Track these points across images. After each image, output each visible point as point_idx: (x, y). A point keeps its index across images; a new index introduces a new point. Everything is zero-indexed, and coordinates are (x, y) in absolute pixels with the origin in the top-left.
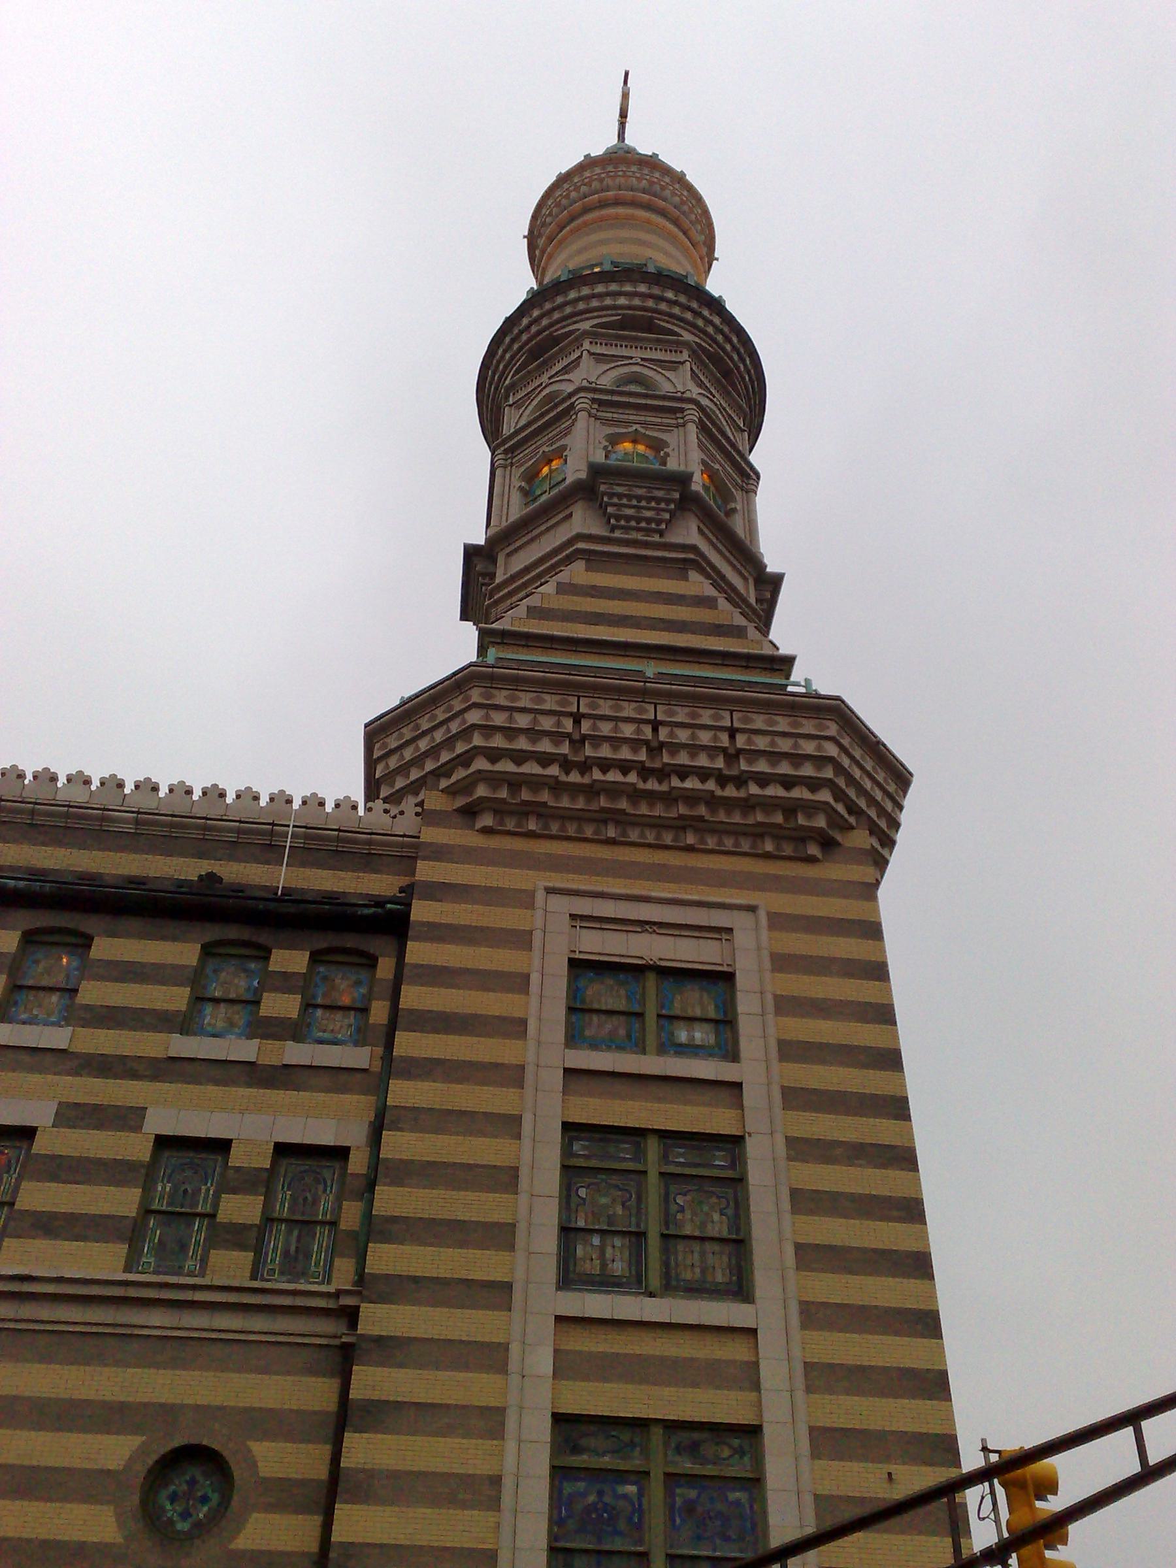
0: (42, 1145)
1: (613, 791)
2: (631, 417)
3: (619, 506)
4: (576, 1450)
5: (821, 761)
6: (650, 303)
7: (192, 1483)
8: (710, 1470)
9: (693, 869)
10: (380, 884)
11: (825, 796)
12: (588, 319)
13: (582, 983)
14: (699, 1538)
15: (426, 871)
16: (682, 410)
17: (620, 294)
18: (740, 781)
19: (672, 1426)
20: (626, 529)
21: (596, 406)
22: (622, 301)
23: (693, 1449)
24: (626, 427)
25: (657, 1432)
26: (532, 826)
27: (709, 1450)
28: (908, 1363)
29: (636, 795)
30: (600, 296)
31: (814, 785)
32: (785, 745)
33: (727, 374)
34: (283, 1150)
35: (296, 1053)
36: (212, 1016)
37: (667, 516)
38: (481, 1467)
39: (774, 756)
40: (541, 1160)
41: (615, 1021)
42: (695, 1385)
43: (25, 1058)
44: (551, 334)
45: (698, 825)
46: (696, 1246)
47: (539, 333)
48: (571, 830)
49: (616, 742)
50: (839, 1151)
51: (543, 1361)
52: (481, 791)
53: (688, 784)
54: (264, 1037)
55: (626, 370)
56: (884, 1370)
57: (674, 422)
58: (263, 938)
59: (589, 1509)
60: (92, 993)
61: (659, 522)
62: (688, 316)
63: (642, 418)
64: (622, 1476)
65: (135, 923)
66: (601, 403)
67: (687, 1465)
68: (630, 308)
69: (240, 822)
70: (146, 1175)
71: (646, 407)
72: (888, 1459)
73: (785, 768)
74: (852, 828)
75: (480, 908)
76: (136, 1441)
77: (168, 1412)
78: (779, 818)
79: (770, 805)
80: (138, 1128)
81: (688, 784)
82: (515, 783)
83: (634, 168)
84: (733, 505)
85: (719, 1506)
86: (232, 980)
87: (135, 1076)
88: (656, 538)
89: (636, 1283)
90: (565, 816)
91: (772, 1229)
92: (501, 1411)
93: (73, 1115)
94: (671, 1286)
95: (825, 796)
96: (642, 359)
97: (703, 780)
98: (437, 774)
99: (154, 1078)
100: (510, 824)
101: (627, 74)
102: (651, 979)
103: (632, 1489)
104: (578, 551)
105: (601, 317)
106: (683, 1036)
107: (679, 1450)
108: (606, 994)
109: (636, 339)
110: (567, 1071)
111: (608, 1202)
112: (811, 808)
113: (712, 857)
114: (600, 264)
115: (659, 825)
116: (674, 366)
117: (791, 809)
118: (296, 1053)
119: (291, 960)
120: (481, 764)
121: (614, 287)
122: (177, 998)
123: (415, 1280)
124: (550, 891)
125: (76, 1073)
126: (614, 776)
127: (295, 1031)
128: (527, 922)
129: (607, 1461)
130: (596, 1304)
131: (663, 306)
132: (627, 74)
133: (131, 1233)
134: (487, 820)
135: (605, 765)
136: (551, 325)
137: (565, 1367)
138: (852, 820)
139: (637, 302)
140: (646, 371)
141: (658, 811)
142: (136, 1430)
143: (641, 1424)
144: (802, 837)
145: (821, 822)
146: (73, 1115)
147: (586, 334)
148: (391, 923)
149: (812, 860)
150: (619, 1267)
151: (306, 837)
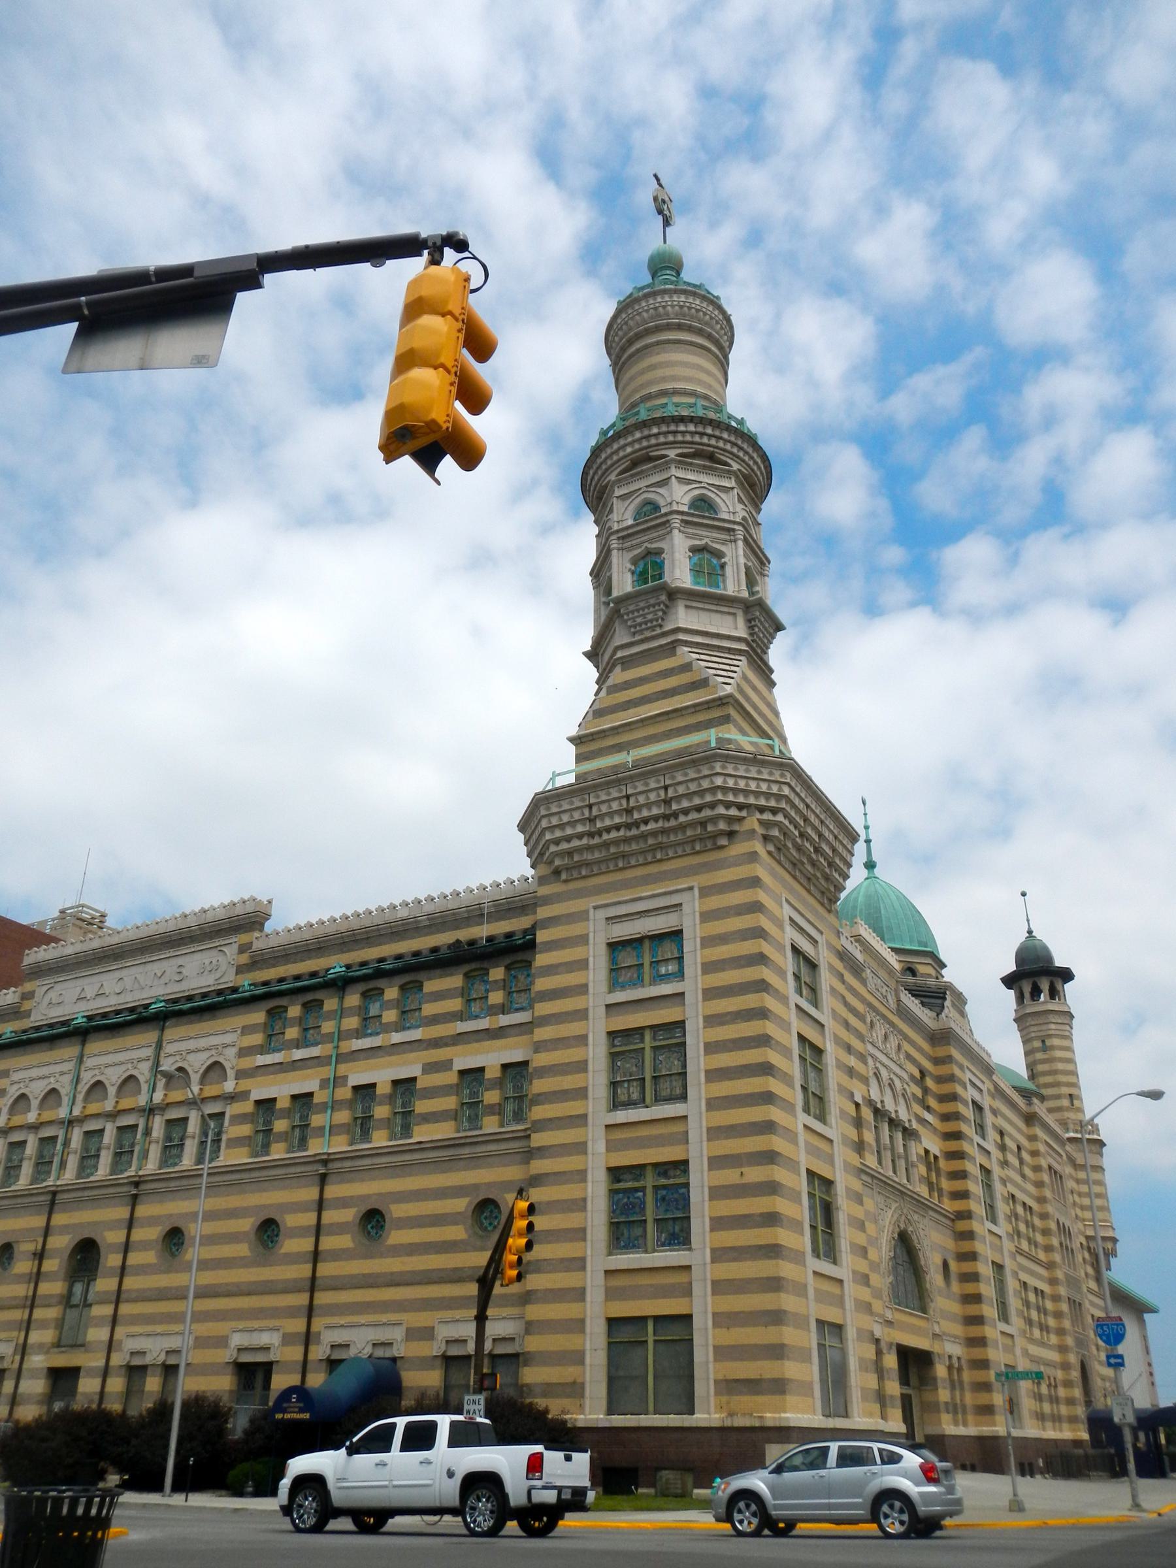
0: (420, 1084)
1: (616, 842)
3: (634, 619)
4: (619, 1181)
7: (491, 1212)
8: (671, 1181)
9: (665, 872)
10: (523, 922)
13: (616, 954)
14: (667, 1210)
15: (543, 913)
16: (734, 530)
17: (626, 445)
18: (675, 815)
19: (655, 1165)
20: (641, 632)
22: (629, 450)
23: (665, 1174)
25: (649, 1168)
26: (584, 873)
27: (671, 1173)
28: (754, 1119)
29: (627, 840)
32: (693, 787)
33: (711, 457)
34: (505, 1067)
35: (505, 1020)
36: (475, 1008)
37: (660, 613)
38: (577, 1194)
39: (689, 796)
40: (597, 1052)
41: (632, 970)
42: (663, 1146)
43: (407, 1046)
45: (661, 847)
46: (668, 1079)
48: (604, 869)
49: (611, 814)
50: (728, 1018)
51: (601, 1147)
53: (649, 827)
54: (491, 1015)
56: (741, 1125)
58: (485, 965)
59: (626, 1204)
60: (429, 1009)
62: (671, 438)
64: (636, 1190)
65: (438, 972)
66: (623, 538)
67: (663, 1181)
70: (455, 1089)
71: (648, 529)
72: (741, 1166)
73: (697, 801)
75: (566, 927)
76: (355, 1210)
77: (476, 1187)
79: (692, 824)
80: (451, 1069)
81: (649, 827)
82: (570, 853)
85: (676, 1196)
86: (478, 990)
87: (447, 1045)
88: (658, 631)
89: (642, 1102)
90: (599, 862)
91: (697, 1062)
92: (586, 1171)
93: (430, 1068)
94: (658, 1099)
98: (762, 810)
99: (454, 1044)
100: (575, 875)
101: (656, 176)
102: (647, 943)
103: (640, 1194)
106: (663, 970)
107: (659, 1175)
108: (627, 958)
109: (642, 472)
110: (607, 1006)
111: (629, 1065)
112: (714, 820)
113: (673, 861)
114: (613, 425)
115: (643, 852)
117: (703, 824)
118: (505, 1020)
119: (497, 973)
120: (553, 848)
122: (455, 1004)
123: (550, 1120)
124: (595, 908)
125: (426, 1049)
126: (614, 834)
127: (503, 1009)
128: (589, 926)
129: (629, 1185)
130: (622, 1116)
132: (656, 176)
133: (454, 1115)
134: (564, 876)
137: (611, 1147)
138: (744, 813)
139: (637, 446)
140: (710, 494)
142: (467, 1196)
143: (642, 1167)
144: (715, 836)
146: (430, 1068)
148: (530, 946)
150: (635, 1096)
151: (494, 906)
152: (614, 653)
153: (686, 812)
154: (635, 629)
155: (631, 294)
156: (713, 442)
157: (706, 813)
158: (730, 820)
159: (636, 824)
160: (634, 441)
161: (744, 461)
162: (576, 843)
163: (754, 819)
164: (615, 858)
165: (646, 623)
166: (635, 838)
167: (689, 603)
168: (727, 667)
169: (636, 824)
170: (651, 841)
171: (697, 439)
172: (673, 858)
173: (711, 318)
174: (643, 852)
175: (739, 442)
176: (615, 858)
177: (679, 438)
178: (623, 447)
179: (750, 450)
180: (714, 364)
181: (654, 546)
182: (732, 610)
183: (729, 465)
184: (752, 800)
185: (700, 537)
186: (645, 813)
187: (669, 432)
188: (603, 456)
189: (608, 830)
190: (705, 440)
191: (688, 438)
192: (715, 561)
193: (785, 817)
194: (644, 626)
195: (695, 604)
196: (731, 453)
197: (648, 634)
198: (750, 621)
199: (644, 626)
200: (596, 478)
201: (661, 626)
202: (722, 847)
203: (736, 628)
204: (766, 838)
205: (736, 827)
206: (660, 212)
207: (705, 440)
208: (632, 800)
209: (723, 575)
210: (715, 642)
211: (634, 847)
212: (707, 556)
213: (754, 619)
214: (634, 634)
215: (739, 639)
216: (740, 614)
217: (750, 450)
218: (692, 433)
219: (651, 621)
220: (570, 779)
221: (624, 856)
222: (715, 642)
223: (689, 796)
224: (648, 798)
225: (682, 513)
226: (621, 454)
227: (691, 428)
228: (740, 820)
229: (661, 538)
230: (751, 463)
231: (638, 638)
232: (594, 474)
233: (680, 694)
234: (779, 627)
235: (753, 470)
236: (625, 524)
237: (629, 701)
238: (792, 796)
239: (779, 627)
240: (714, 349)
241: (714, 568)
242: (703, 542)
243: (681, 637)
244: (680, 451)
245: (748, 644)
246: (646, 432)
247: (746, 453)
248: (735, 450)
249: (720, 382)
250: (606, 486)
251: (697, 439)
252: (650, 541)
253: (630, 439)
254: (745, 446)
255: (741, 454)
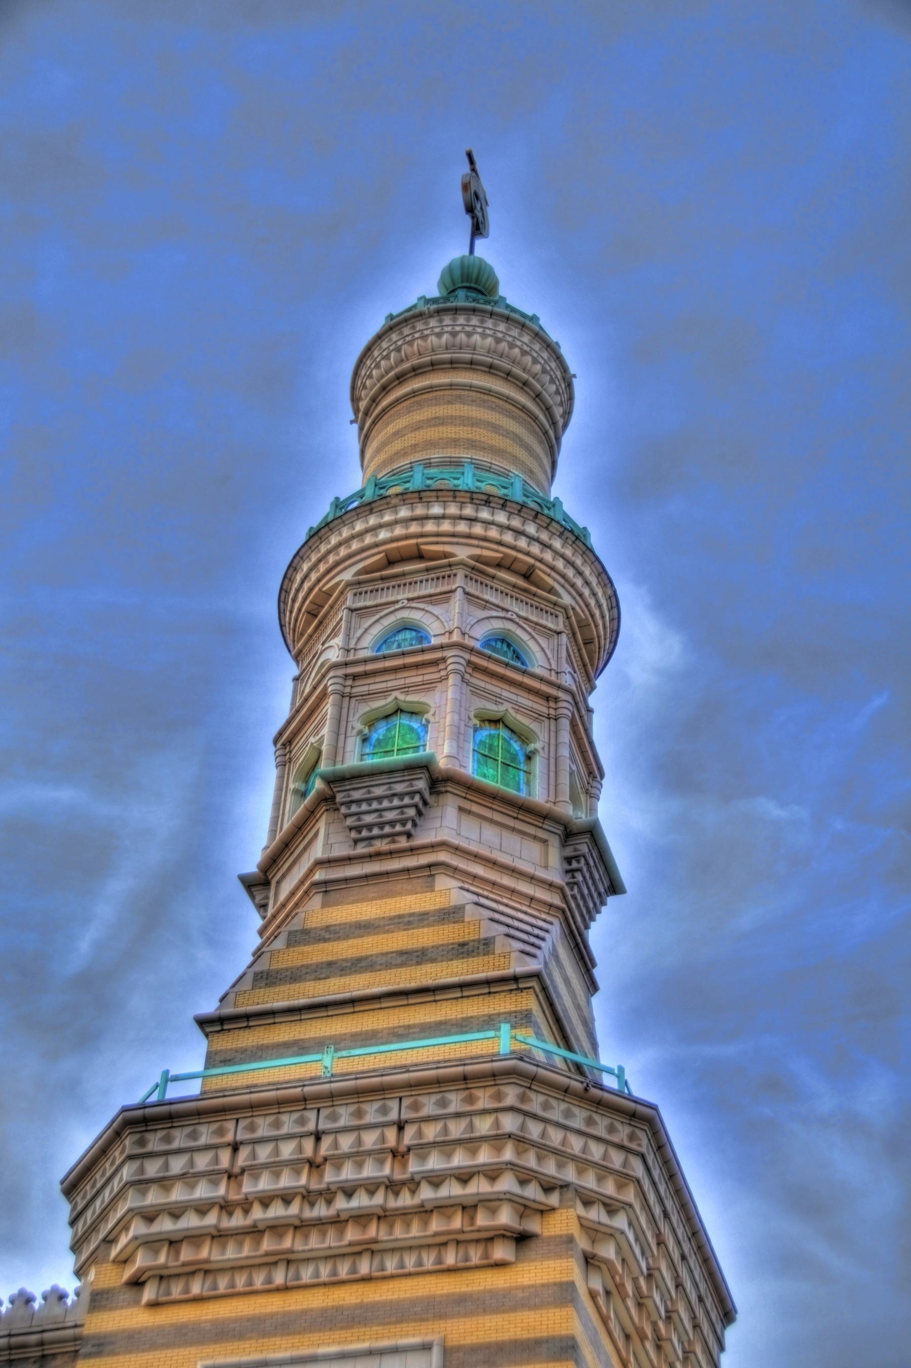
2: (390, 684)
5: (498, 1139)
6: (414, 528)
11: (507, 1184)
12: (345, 569)
16: (556, 699)
18: (413, 1184)
21: (349, 682)
22: (383, 535)
24: (385, 697)
29: (301, 1227)
30: (361, 535)
31: (492, 1173)
32: (457, 1129)
37: (411, 812)
44: (320, 590)
45: (370, 1249)
47: (311, 590)
52: (141, 1260)
53: (354, 1203)
55: (391, 619)
57: (437, 676)
61: (403, 822)
62: (462, 527)
63: (401, 682)
66: (476, 668)
68: (392, 540)
69: (435, 1001)
71: (405, 667)
74: (553, 1209)
78: (457, 1222)
79: (443, 1208)
81: (354, 1203)
83: (433, 323)
84: (532, 746)
88: (403, 843)
95: (507, 1184)
96: (409, 600)
97: (371, 1193)
101: (470, 155)
104: (316, 884)
105: (362, 560)
112: (490, 1203)
115: (333, 1257)
116: (444, 597)
117: (469, 1208)
121: (373, 521)
126: (277, 1211)
131: (430, 527)
132: (470, 155)
134: (149, 1293)
135: (265, 1201)
136: (319, 581)
138: (554, 1199)
139: (399, 531)
140: (519, 632)
141: (331, 1240)
145: (505, 1217)
147: (349, 584)
149: (501, 1265)
152: (311, 871)
153: (436, 1180)
154: (360, 833)
155: (415, 306)
156: (535, 549)
157: (480, 1187)
158: (525, 1209)
159: (328, 1195)
160: (396, 522)
161: (581, 595)
162: (191, 1221)
163: (572, 1213)
164: (270, 1262)
165: (381, 825)
166: (320, 1224)
167: (466, 805)
168: (529, 929)
169: (328, 1195)
170: (352, 1234)
171: (508, 537)
172: (393, 1277)
173: (544, 371)
174: (333, 1257)
175: (579, 562)
176: (270, 1262)
177: (478, 529)
178: (374, 529)
179: (593, 580)
180: (541, 442)
181: (411, 698)
182: (541, 834)
183: (558, 595)
184: (570, 1174)
185: (497, 699)
186: (348, 1173)
187: (461, 518)
188: (334, 540)
189: (265, 1201)
190: (522, 543)
191: (493, 533)
192: (516, 746)
193: (630, 1224)
194: (376, 831)
195: (475, 808)
196: (563, 576)
197: (381, 845)
198: (569, 860)
199: (376, 831)
200: (314, 577)
201: (409, 835)
202: (501, 1265)
203: (546, 867)
204: (589, 1261)
205: (534, 1225)
206: (470, 209)
207: (522, 543)
208: (326, 1142)
209: (528, 773)
210: (506, 881)
211: (314, 1242)
212: (503, 733)
213: (577, 858)
214: (356, 842)
215: (551, 885)
216: (554, 842)
217: (593, 580)
218: (502, 527)
219: (392, 823)
220: (194, 1088)
221: (289, 1260)
222: (506, 881)
223: (446, 1146)
224: (359, 1142)
225: (472, 650)
226: (368, 540)
227: (501, 517)
228: (544, 1211)
229: (428, 687)
230: (592, 602)
231: (361, 850)
232: (311, 570)
233: (433, 960)
234: (615, 887)
235: (592, 616)
236: (362, 654)
237: (330, 964)
238: (646, 1184)
239: (615, 887)
240: (542, 417)
241: (514, 758)
242: (501, 708)
243: (443, 856)
244: (478, 552)
245: (565, 898)
246: (420, 511)
247: (587, 583)
248: (570, 573)
249: (545, 472)
250: (329, 594)
251: (508, 537)
252: (406, 689)
253: (388, 518)
254: (587, 571)
255: (579, 582)
